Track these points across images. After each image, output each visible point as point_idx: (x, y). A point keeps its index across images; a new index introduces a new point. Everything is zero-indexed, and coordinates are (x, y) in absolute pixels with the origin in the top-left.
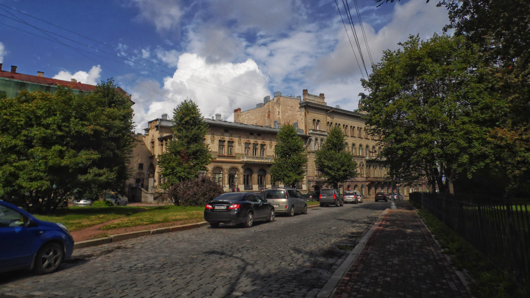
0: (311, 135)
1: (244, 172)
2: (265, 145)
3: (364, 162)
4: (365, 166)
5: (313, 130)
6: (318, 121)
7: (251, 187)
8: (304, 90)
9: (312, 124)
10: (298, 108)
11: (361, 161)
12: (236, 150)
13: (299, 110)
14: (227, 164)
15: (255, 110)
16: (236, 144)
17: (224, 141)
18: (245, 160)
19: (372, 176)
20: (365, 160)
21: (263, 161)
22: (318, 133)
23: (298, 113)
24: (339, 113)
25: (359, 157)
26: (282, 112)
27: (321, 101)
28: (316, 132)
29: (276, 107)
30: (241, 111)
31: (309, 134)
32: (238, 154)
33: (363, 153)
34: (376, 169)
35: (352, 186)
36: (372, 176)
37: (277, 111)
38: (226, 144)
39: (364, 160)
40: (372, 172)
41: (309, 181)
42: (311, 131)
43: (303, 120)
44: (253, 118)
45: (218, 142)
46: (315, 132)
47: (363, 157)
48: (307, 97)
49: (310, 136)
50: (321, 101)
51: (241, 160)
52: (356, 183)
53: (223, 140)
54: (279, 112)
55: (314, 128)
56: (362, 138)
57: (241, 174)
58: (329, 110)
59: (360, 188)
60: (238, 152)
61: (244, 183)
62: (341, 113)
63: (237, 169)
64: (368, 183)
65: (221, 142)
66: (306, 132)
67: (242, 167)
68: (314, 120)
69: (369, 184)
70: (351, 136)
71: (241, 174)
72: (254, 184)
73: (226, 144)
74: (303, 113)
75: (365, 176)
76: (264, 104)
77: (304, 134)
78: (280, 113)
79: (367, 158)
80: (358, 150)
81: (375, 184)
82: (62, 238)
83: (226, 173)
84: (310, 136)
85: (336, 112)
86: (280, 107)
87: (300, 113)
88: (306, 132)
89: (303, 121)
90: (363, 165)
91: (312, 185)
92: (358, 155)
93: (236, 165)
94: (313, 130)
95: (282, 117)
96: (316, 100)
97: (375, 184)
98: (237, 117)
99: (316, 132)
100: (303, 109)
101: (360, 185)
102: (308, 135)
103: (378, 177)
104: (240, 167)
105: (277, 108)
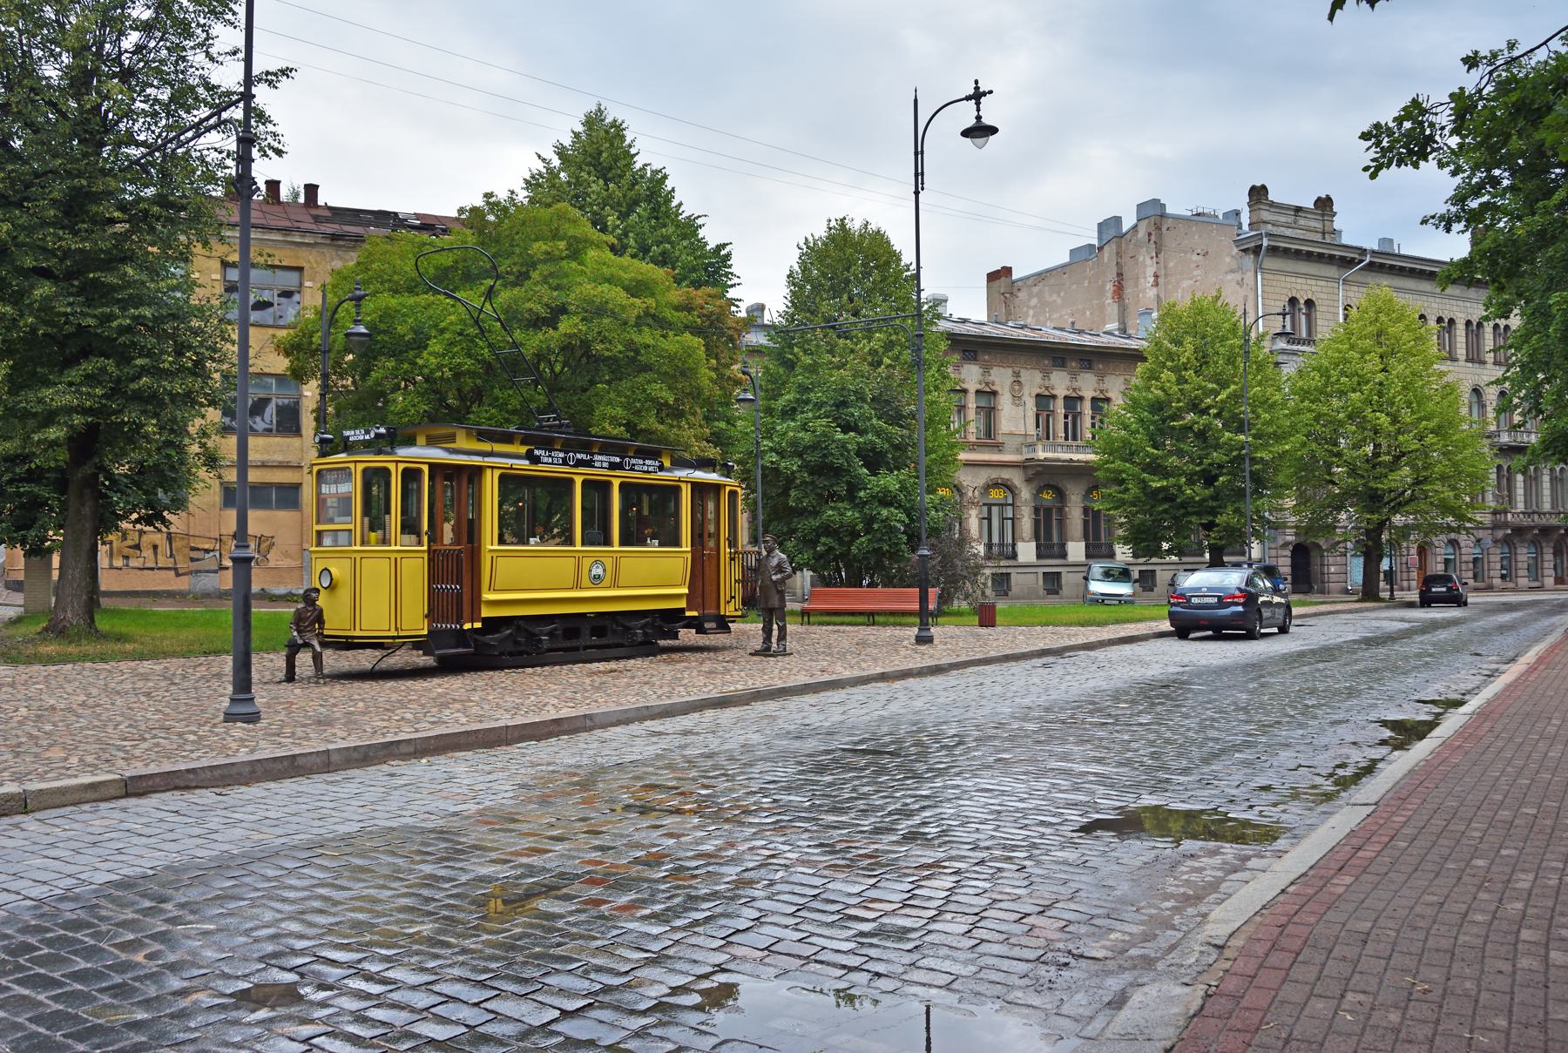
6: (1310, 303)
14: (976, 469)
16: (1005, 403)
20: (1492, 446)
23: (1229, 277)
24: (1392, 267)
62: (1402, 269)
65: (1043, 400)
67: (1028, 480)
87: (1238, 276)
93: (1006, 474)
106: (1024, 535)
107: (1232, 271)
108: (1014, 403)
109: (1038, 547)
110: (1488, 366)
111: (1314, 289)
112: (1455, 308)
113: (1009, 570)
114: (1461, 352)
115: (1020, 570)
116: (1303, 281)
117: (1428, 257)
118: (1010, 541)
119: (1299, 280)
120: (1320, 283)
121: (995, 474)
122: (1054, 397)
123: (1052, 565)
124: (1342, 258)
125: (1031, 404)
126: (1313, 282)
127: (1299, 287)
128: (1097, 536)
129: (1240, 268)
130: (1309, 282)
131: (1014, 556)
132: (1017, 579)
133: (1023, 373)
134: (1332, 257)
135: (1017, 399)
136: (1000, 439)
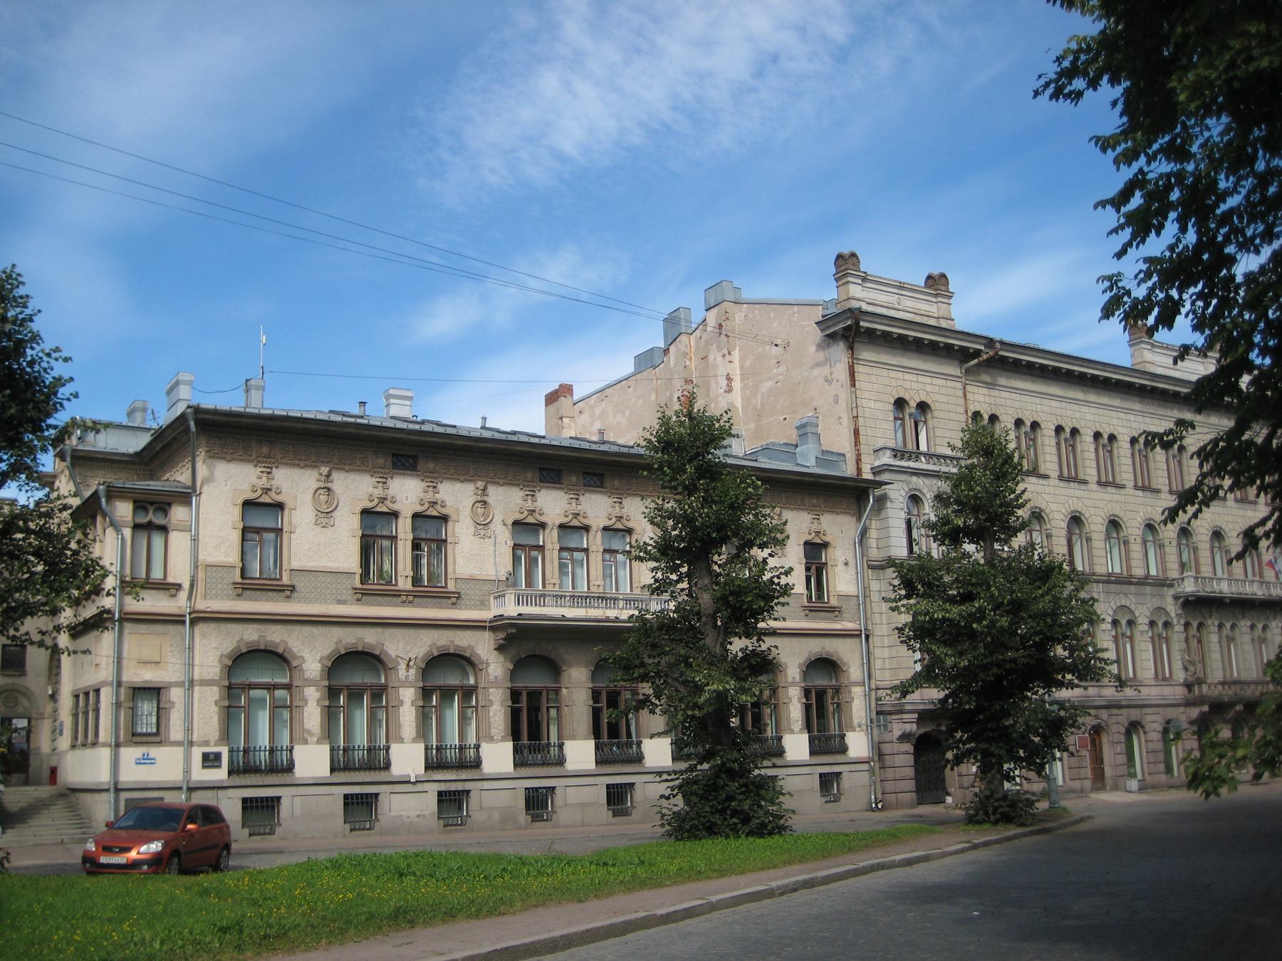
0: (885, 477)
1: (513, 674)
2: (825, 545)
3: (1173, 609)
4: (1179, 628)
5: (897, 453)
6: (923, 407)
7: (554, 751)
8: (840, 257)
9: (890, 426)
10: (813, 349)
11: (1156, 603)
12: (460, 561)
13: (821, 356)
14: (411, 632)
15: (631, 382)
16: (462, 534)
17: (395, 515)
18: (511, 609)
19: (1216, 675)
20: (1176, 598)
21: (612, 613)
22: (923, 464)
23: (816, 372)
24: (1030, 365)
25: (1144, 581)
26: (744, 376)
27: (933, 309)
28: (911, 464)
29: (715, 357)
30: (577, 396)
31: (876, 471)
32: (472, 580)
33: (1091, 556)
34: (1231, 639)
35: (1114, 728)
36: (1216, 675)
37: (722, 372)
38: (550, 539)
39: (1170, 600)
40: (1215, 655)
41: (878, 713)
42: (886, 458)
43: (843, 404)
44: (624, 422)
45: (356, 520)
46: (903, 463)
47: (1163, 583)
48: (855, 290)
49: (881, 484)
50: (933, 309)
51: (487, 615)
52: (1134, 714)
53: (531, 520)
54: (729, 379)
55: (900, 445)
56: (1158, 491)
57: (496, 684)
58: (977, 353)
59: (1156, 736)
60: (476, 573)
61: (515, 734)
62: (1043, 368)
63: (469, 661)
64: (1195, 712)
65: (526, 527)
66: (858, 461)
67: (500, 649)
68: (900, 404)
69: (1203, 714)
70: (1099, 483)
71: (496, 684)
72: (574, 738)
73: (550, 539)
74: (841, 371)
75: (1180, 676)
76: (666, 351)
77: (849, 470)
78: (737, 384)
79: (1189, 587)
80: (1136, 548)
81: (1231, 714)
82: (90, 852)
83: (406, 684)
84: (881, 484)
85: (1017, 362)
86: (736, 354)
87: (825, 371)
88: (858, 461)
89: (842, 410)
90: (1167, 624)
91: (897, 729)
92: (1138, 572)
93: (462, 640)
94: (897, 453)
95: (746, 400)
96: (909, 303)
97: (1231, 714)
98: (556, 420)
99: (911, 464)
100: (839, 351)
101: (1153, 722)
102: (867, 475)
103: (1244, 677)
104: (483, 647)
105: (719, 358)
106: (493, 731)
107: (818, 365)
108: (476, 534)
109: (516, 750)
110: (1162, 495)
111: (929, 388)
112: (1115, 421)
113: (468, 786)
114: (1090, 472)
115: (487, 785)
116: (914, 377)
117: (1085, 357)
118: (383, 742)
119: (907, 377)
120: (936, 381)
121: (251, 635)
122: (395, 515)
123: (828, 765)
124: (963, 350)
125: (504, 538)
126: (928, 380)
127: (908, 385)
128: (823, 727)
129: (827, 360)
130: (921, 379)
131: (477, 764)
132: (291, 804)
133: (492, 490)
134: (949, 347)
135: (482, 525)
136: (834, 602)
